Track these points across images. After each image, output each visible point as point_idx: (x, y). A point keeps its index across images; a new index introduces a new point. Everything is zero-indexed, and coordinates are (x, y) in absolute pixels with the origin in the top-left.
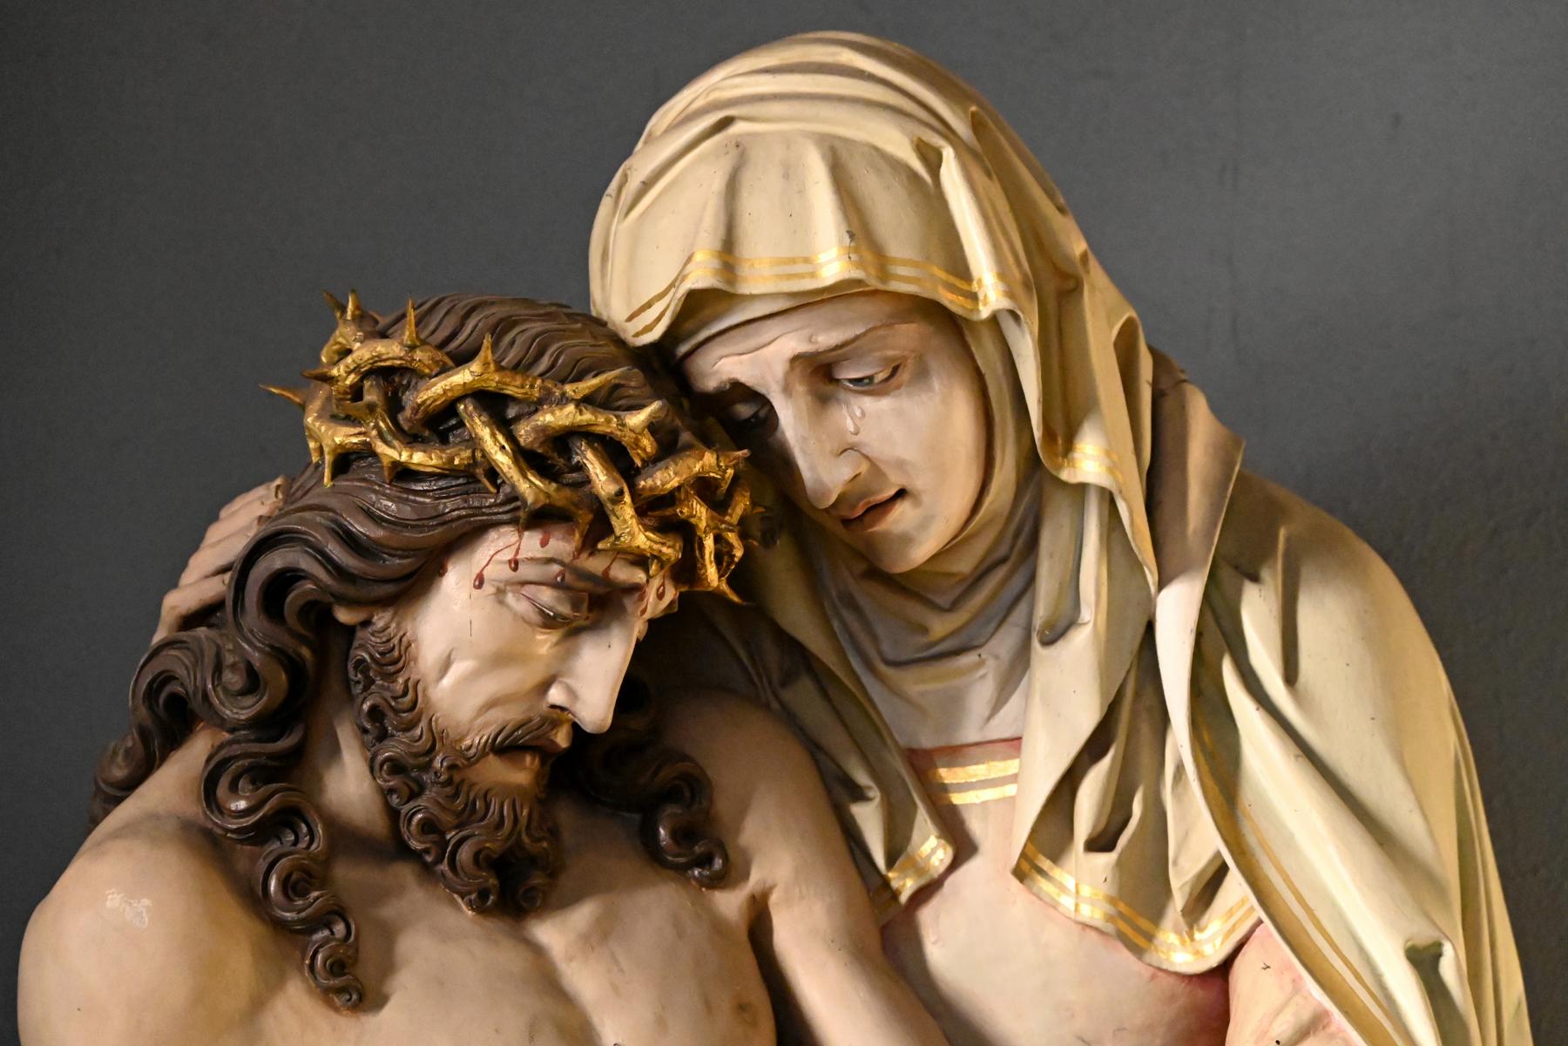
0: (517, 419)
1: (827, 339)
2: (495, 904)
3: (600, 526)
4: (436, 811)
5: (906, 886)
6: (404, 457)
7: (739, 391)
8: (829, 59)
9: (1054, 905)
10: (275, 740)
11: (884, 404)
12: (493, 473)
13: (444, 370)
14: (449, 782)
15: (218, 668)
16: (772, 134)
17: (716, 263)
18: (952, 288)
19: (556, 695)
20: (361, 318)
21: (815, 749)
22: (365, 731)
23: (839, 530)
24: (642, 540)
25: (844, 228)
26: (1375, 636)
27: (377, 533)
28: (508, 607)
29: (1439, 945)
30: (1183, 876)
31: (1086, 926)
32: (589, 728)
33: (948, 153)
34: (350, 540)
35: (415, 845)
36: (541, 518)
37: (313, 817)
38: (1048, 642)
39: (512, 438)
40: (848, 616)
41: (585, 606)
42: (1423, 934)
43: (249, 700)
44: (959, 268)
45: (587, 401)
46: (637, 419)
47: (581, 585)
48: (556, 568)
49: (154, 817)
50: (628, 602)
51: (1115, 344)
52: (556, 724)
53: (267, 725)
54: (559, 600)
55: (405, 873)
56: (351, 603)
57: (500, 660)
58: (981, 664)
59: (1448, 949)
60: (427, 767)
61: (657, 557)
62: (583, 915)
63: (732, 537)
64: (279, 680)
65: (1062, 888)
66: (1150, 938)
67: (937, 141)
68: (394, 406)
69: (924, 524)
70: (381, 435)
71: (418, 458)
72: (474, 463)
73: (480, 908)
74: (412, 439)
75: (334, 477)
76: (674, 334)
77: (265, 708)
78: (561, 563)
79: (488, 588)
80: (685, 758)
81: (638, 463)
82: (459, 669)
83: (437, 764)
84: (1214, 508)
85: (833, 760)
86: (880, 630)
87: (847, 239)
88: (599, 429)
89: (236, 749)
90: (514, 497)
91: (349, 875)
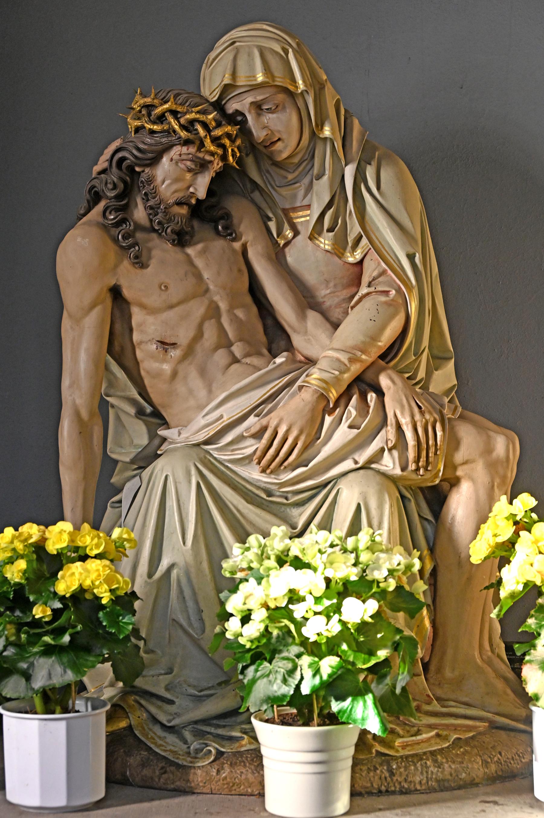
0: (180, 117)
1: (259, 98)
2: (177, 244)
3: (202, 145)
4: (161, 219)
5: (282, 242)
6: (152, 127)
7: (238, 113)
8: (260, 28)
9: (319, 246)
10: (121, 201)
11: (274, 116)
12: (174, 131)
13: (162, 105)
14: (165, 212)
15: (106, 184)
16: (246, 45)
17: (231, 77)
18: (291, 85)
19: (191, 190)
20: (141, 94)
21: (259, 208)
22: (143, 199)
23: (264, 150)
24: (212, 148)
25: (263, 68)
26: (400, 178)
27: (146, 147)
28: (179, 167)
29: (415, 254)
30: (350, 240)
31: (327, 251)
32: (200, 198)
33: (290, 50)
34: (139, 149)
35: (157, 228)
36: (187, 142)
37: (130, 220)
38: (317, 179)
39: (179, 122)
40: (267, 175)
41: (199, 166)
42: (411, 251)
43: (114, 191)
44: (294, 80)
45: (198, 112)
46: (211, 117)
47: (197, 160)
48: (191, 156)
49: (90, 221)
50: (209, 165)
51: (335, 105)
52: (191, 197)
53: (118, 197)
54: (191, 164)
55: (154, 235)
56: (139, 166)
57: (177, 180)
58: (301, 186)
59: (417, 255)
60: (159, 208)
61: (216, 153)
62: (200, 246)
63: (236, 150)
64: (121, 186)
65: (321, 242)
66: (343, 254)
67: (288, 47)
68: (149, 115)
69: (285, 147)
70: (146, 122)
71: (155, 127)
72: (170, 129)
73: (173, 245)
74: (154, 123)
75: (135, 134)
76: (220, 98)
77: (118, 193)
78: (192, 154)
79: (174, 162)
80: (226, 209)
81: (211, 128)
82: (167, 182)
83: (162, 207)
84: (359, 146)
85: (263, 211)
86: (276, 179)
87: (264, 71)
88: (201, 119)
89: (111, 204)
90: (180, 137)
91: (139, 235)
